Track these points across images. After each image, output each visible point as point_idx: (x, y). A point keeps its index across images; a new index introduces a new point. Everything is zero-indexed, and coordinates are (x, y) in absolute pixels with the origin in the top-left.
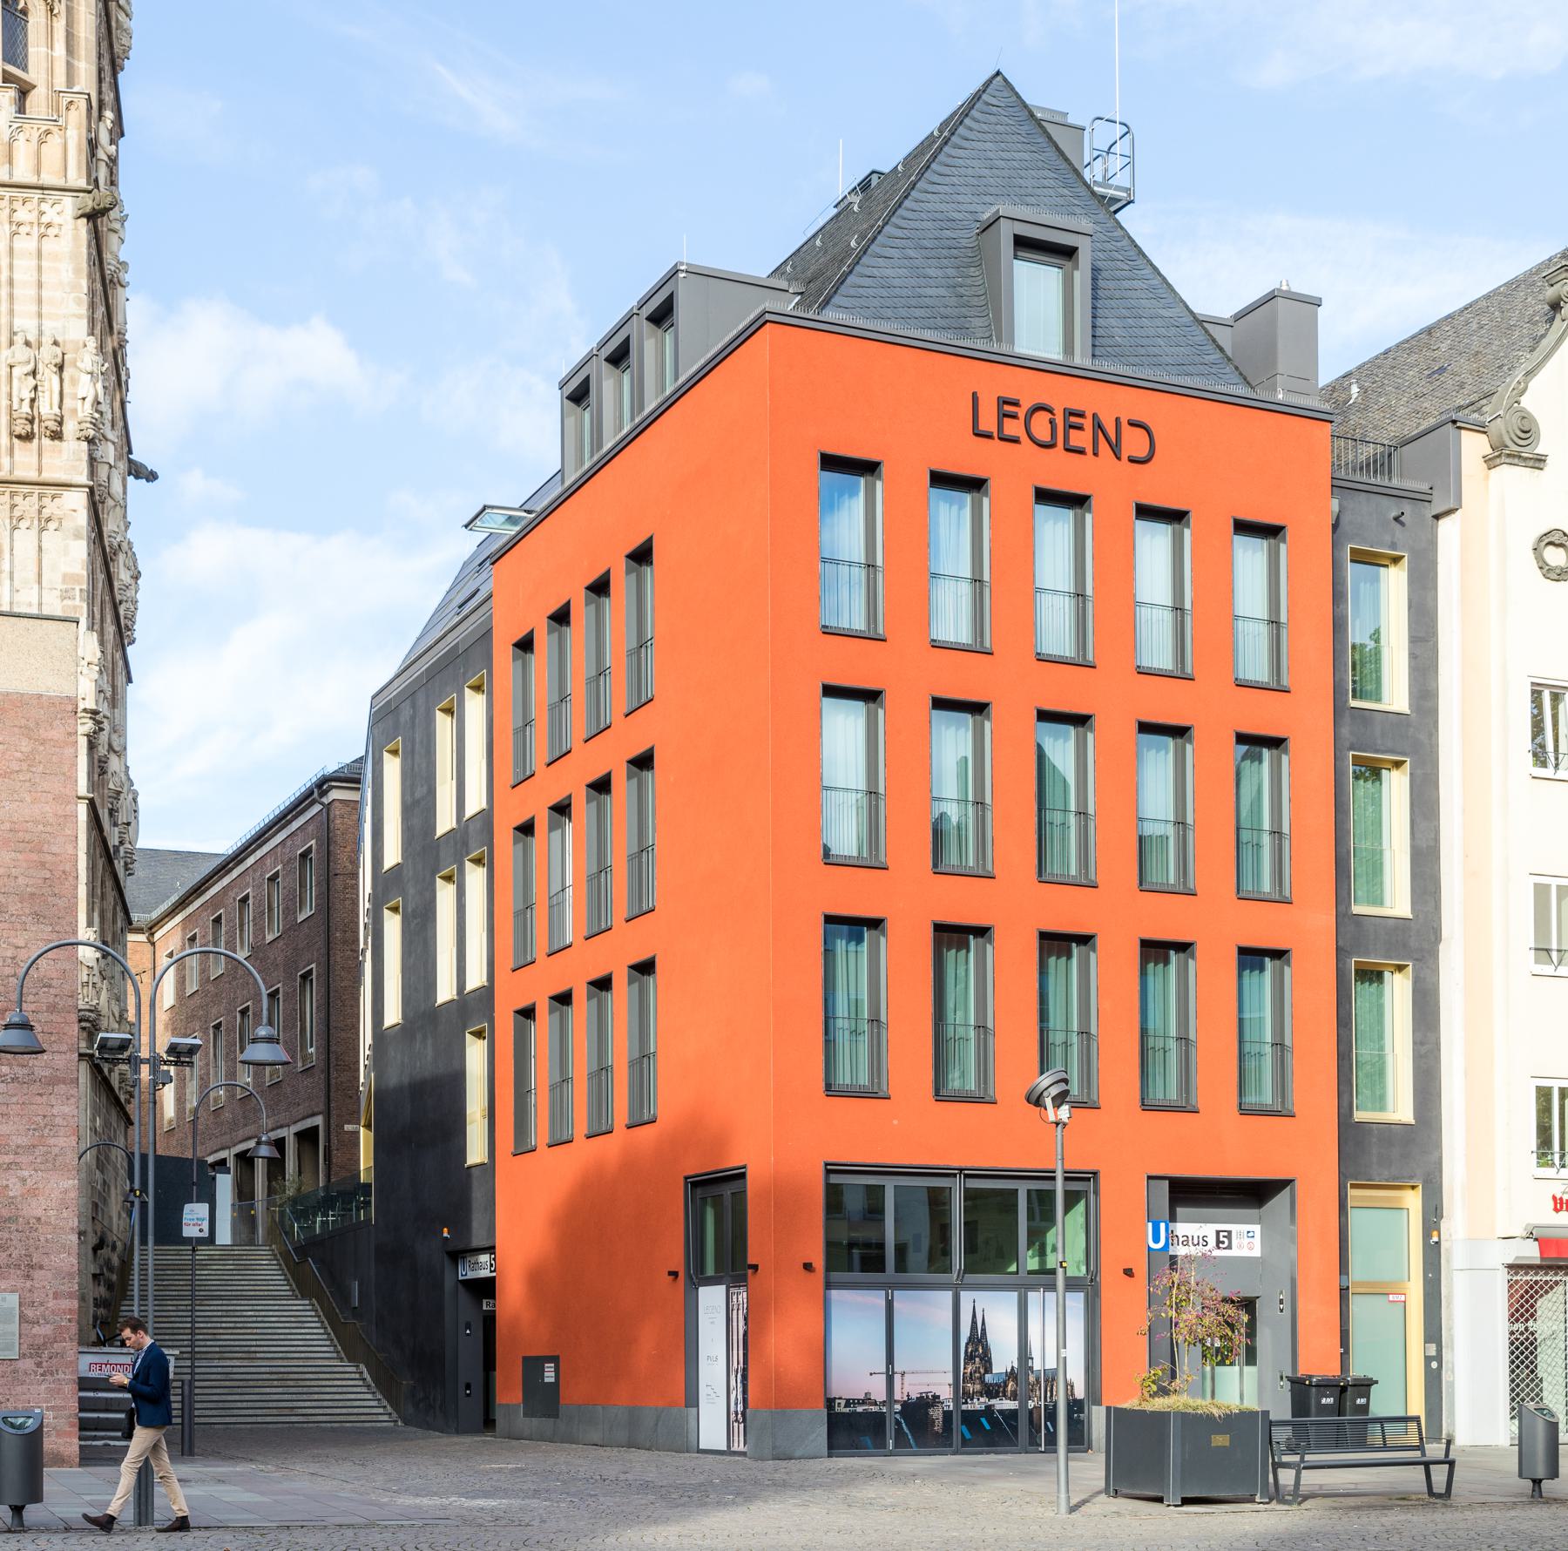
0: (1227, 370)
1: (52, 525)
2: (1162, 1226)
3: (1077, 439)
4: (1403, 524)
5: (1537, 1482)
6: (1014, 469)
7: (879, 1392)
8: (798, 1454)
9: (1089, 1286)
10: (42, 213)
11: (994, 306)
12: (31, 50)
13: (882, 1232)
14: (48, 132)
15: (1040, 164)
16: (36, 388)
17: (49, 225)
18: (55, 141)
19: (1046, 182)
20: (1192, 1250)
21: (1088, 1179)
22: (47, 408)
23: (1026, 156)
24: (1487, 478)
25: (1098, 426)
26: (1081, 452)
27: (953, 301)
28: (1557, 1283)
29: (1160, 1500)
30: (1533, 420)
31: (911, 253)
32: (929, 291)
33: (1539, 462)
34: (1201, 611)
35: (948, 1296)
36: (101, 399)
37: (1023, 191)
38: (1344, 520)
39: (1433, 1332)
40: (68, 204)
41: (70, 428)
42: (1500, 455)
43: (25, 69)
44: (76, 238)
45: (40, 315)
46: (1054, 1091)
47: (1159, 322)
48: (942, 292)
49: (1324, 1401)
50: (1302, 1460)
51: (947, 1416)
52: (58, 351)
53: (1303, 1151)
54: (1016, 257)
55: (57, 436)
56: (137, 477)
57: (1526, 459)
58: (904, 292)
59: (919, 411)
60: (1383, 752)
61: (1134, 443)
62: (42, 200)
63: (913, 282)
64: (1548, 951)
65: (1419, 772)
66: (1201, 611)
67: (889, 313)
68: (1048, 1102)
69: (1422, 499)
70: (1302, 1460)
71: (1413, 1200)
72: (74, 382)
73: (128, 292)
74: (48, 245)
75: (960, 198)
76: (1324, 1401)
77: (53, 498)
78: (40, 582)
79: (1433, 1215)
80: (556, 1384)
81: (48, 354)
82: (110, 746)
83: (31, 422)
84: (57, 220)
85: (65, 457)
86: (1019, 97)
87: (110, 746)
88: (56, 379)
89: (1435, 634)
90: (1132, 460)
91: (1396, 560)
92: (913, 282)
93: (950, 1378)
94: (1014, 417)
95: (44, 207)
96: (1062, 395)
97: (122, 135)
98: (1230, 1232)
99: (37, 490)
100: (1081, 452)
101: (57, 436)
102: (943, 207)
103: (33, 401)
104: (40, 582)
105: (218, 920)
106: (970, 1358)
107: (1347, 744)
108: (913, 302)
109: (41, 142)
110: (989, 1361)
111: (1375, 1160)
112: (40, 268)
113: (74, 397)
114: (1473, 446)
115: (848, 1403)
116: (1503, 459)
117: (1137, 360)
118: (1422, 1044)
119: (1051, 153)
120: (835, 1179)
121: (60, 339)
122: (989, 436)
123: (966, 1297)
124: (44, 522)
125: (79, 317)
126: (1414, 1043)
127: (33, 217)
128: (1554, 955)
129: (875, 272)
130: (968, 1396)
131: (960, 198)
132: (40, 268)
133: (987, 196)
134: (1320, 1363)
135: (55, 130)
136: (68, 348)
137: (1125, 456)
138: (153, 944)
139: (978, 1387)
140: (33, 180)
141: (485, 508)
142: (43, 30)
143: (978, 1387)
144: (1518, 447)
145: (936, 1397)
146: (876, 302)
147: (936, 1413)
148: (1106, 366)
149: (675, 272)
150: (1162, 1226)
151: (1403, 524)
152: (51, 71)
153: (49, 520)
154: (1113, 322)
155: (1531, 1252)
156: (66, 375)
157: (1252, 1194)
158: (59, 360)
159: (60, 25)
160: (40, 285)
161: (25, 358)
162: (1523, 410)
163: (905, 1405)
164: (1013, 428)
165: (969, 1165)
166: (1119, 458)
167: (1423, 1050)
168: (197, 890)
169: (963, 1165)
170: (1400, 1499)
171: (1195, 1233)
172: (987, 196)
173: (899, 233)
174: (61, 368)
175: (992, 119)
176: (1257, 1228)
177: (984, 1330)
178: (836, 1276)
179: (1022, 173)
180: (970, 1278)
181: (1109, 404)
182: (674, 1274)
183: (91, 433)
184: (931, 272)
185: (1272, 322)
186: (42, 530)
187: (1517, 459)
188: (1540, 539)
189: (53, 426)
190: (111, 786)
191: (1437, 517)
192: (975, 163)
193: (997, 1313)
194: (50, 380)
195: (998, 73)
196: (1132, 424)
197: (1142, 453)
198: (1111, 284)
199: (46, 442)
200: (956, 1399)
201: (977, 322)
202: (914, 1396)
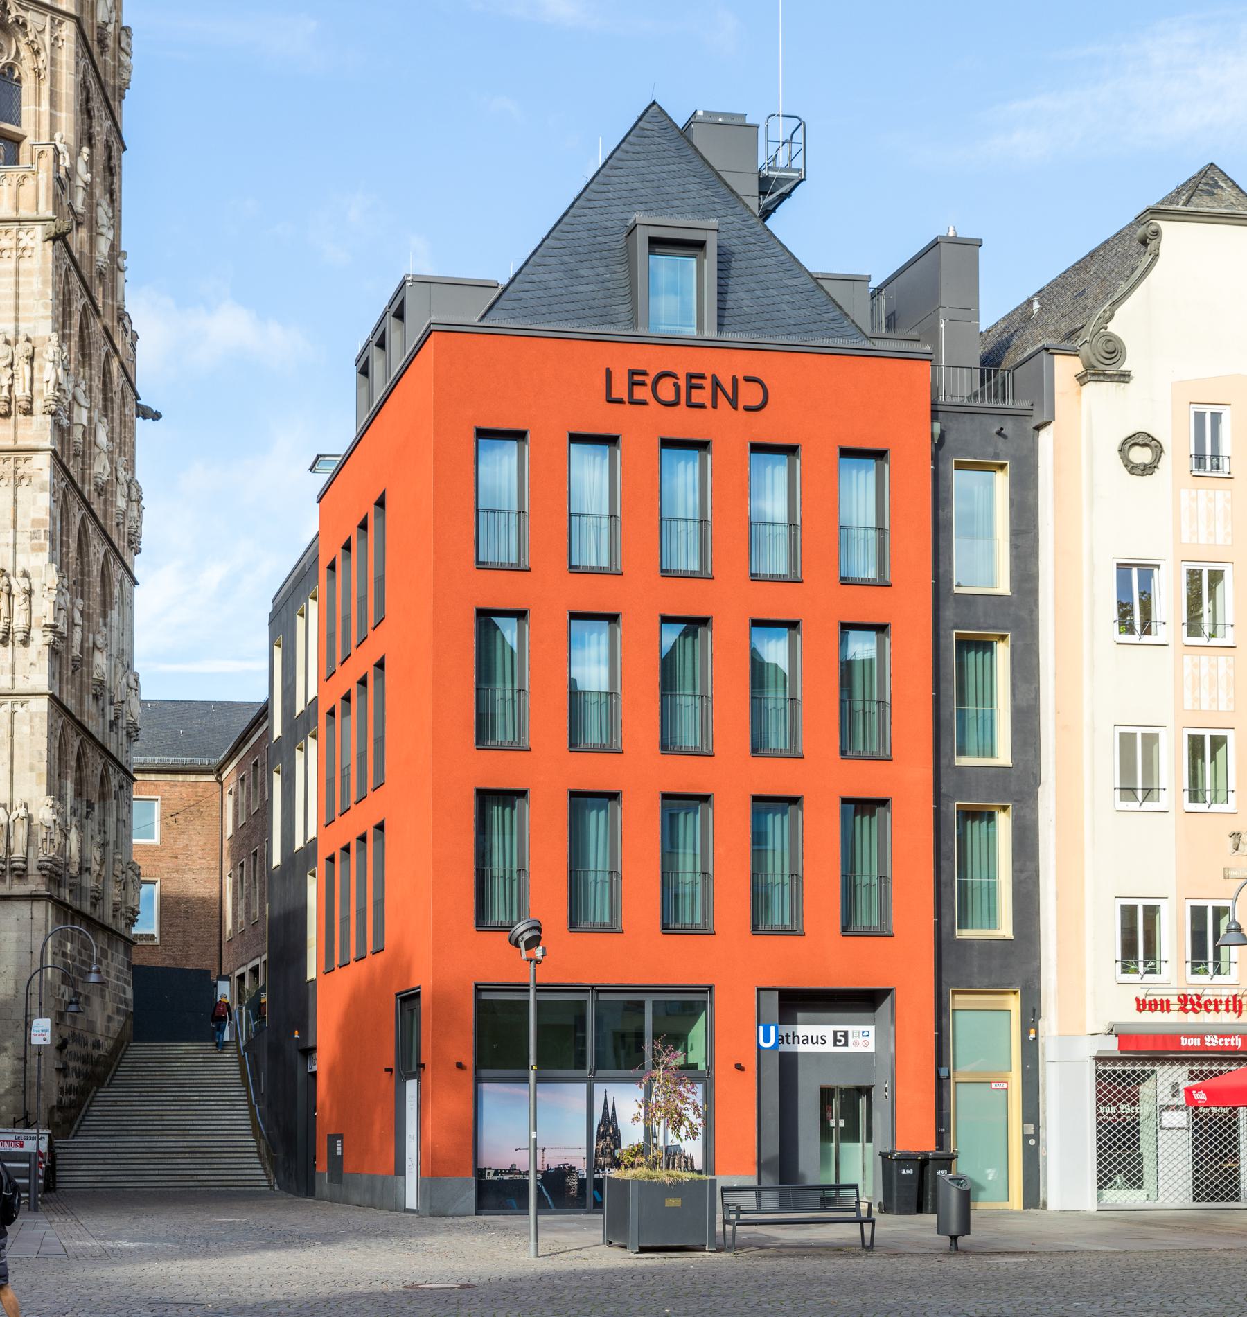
0: (845, 324)
1: (24, 482)
2: (772, 1029)
3: (697, 396)
4: (1005, 437)
5: (954, 1238)
6: (642, 426)
7: (522, 1160)
8: (450, 1212)
9: (708, 1079)
10: (19, 240)
11: (632, 293)
12: (24, 109)
13: (522, 1035)
14: (24, 177)
15: (686, 173)
16: (12, 376)
17: (24, 249)
18: (30, 183)
19: (691, 187)
20: (809, 1048)
21: (705, 992)
22: (20, 392)
23: (675, 167)
24: (1079, 393)
25: (716, 384)
26: (702, 406)
27: (601, 294)
28: (1153, 1072)
29: (625, 1247)
30: (1120, 341)
31: (567, 259)
32: (580, 288)
33: (1124, 377)
34: (815, 526)
35: (583, 1087)
36: (61, 381)
37: (669, 197)
38: (950, 438)
39: (1032, 1113)
40: (39, 231)
41: (38, 405)
42: (1089, 375)
43: (19, 124)
44: (44, 257)
45: (17, 319)
46: (527, 936)
47: (783, 291)
48: (591, 287)
49: (904, 1172)
50: (738, 1218)
51: (582, 1183)
52: (29, 346)
53: (904, 963)
54: (651, 253)
55: (28, 412)
56: (144, 418)
57: (1110, 376)
58: (559, 291)
59: (568, 384)
60: (985, 629)
61: (749, 395)
62: (19, 230)
63: (567, 282)
64: (1134, 789)
65: (1020, 643)
66: (815, 526)
67: (544, 310)
68: (522, 944)
69: (1025, 415)
70: (738, 1218)
71: (1014, 1003)
72: (41, 369)
73: (127, 275)
74: (24, 264)
75: (613, 209)
76: (904, 1172)
77: (25, 460)
78: (14, 527)
79: (1031, 1015)
80: (341, 1157)
81: (22, 349)
82: (94, 644)
83: (9, 403)
84: (31, 244)
85: (34, 427)
86: (670, 120)
87: (94, 644)
88: (27, 368)
89: (1036, 526)
90: (747, 409)
91: (1002, 467)
92: (567, 282)
93: (584, 1153)
94: (643, 384)
95: (21, 235)
96: (683, 363)
97: (125, 149)
98: (846, 1033)
99: (13, 455)
100: (702, 406)
101: (28, 412)
102: (598, 218)
103: (11, 386)
104: (14, 527)
105: (255, 765)
106: (601, 1137)
107: (951, 625)
108: (565, 299)
109: (19, 185)
110: (619, 1139)
111: (975, 970)
112: (17, 283)
113: (41, 380)
114: (1065, 368)
115: (496, 1172)
116: (1089, 378)
117: (761, 324)
118: (1021, 871)
119: (697, 162)
120: (486, 996)
121: (31, 337)
122: (621, 402)
123: (599, 1088)
124: (18, 480)
125: (46, 318)
126: (1014, 871)
127: (12, 244)
128: (1139, 794)
129: (535, 278)
130: (600, 1167)
131: (613, 209)
132: (17, 283)
133: (685, 189)
134: (919, 1140)
135: (30, 174)
136: (37, 343)
137: (741, 406)
138: (221, 783)
139: (608, 1160)
140: (12, 215)
141: (318, 456)
142: (32, 92)
143: (608, 1160)
144: (1107, 365)
145: (572, 1168)
146: (534, 302)
147: (572, 1181)
148: (727, 336)
149: (404, 282)
150: (772, 1029)
151: (1005, 437)
152: (38, 123)
153: (22, 478)
154: (743, 295)
155: (1111, 1045)
156: (35, 364)
157: (864, 1001)
158: (30, 353)
159: (45, 87)
160: (17, 296)
161: (4, 354)
162: (1110, 334)
163: (545, 1174)
164: (641, 393)
165: (598, 983)
166: (735, 408)
167: (1023, 876)
168: (243, 739)
169: (593, 983)
170: (837, 1250)
171: (815, 1036)
172: (685, 189)
173: (559, 244)
174: (31, 359)
175: (646, 141)
176: (871, 1029)
177: (614, 1114)
178: (485, 1073)
179: (670, 182)
180: (600, 1073)
181: (725, 367)
182: (389, 1070)
183: (53, 408)
184: (583, 273)
185: (937, 264)
186: (16, 486)
187: (1100, 376)
188: (1125, 442)
189: (24, 404)
190: (95, 676)
191: (1038, 428)
192: (630, 179)
193: (626, 1101)
194: (23, 369)
195: (654, 103)
196: (747, 379)
197: (757, 402)
198: (743, 264)
199: (21, 417)
200: (589, 1169)
201: (620, 309)
202: (553, 1167)
